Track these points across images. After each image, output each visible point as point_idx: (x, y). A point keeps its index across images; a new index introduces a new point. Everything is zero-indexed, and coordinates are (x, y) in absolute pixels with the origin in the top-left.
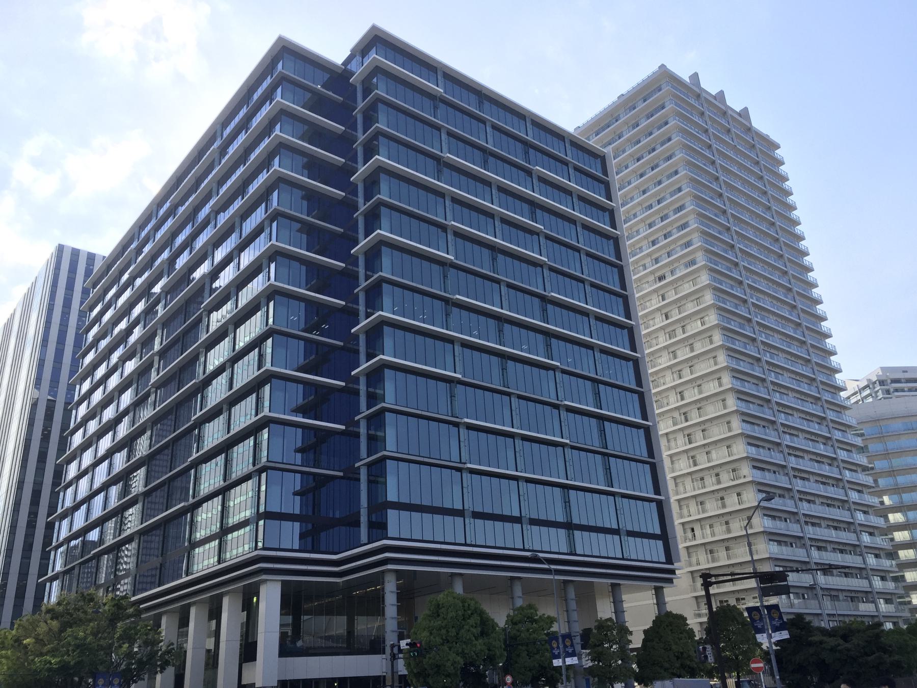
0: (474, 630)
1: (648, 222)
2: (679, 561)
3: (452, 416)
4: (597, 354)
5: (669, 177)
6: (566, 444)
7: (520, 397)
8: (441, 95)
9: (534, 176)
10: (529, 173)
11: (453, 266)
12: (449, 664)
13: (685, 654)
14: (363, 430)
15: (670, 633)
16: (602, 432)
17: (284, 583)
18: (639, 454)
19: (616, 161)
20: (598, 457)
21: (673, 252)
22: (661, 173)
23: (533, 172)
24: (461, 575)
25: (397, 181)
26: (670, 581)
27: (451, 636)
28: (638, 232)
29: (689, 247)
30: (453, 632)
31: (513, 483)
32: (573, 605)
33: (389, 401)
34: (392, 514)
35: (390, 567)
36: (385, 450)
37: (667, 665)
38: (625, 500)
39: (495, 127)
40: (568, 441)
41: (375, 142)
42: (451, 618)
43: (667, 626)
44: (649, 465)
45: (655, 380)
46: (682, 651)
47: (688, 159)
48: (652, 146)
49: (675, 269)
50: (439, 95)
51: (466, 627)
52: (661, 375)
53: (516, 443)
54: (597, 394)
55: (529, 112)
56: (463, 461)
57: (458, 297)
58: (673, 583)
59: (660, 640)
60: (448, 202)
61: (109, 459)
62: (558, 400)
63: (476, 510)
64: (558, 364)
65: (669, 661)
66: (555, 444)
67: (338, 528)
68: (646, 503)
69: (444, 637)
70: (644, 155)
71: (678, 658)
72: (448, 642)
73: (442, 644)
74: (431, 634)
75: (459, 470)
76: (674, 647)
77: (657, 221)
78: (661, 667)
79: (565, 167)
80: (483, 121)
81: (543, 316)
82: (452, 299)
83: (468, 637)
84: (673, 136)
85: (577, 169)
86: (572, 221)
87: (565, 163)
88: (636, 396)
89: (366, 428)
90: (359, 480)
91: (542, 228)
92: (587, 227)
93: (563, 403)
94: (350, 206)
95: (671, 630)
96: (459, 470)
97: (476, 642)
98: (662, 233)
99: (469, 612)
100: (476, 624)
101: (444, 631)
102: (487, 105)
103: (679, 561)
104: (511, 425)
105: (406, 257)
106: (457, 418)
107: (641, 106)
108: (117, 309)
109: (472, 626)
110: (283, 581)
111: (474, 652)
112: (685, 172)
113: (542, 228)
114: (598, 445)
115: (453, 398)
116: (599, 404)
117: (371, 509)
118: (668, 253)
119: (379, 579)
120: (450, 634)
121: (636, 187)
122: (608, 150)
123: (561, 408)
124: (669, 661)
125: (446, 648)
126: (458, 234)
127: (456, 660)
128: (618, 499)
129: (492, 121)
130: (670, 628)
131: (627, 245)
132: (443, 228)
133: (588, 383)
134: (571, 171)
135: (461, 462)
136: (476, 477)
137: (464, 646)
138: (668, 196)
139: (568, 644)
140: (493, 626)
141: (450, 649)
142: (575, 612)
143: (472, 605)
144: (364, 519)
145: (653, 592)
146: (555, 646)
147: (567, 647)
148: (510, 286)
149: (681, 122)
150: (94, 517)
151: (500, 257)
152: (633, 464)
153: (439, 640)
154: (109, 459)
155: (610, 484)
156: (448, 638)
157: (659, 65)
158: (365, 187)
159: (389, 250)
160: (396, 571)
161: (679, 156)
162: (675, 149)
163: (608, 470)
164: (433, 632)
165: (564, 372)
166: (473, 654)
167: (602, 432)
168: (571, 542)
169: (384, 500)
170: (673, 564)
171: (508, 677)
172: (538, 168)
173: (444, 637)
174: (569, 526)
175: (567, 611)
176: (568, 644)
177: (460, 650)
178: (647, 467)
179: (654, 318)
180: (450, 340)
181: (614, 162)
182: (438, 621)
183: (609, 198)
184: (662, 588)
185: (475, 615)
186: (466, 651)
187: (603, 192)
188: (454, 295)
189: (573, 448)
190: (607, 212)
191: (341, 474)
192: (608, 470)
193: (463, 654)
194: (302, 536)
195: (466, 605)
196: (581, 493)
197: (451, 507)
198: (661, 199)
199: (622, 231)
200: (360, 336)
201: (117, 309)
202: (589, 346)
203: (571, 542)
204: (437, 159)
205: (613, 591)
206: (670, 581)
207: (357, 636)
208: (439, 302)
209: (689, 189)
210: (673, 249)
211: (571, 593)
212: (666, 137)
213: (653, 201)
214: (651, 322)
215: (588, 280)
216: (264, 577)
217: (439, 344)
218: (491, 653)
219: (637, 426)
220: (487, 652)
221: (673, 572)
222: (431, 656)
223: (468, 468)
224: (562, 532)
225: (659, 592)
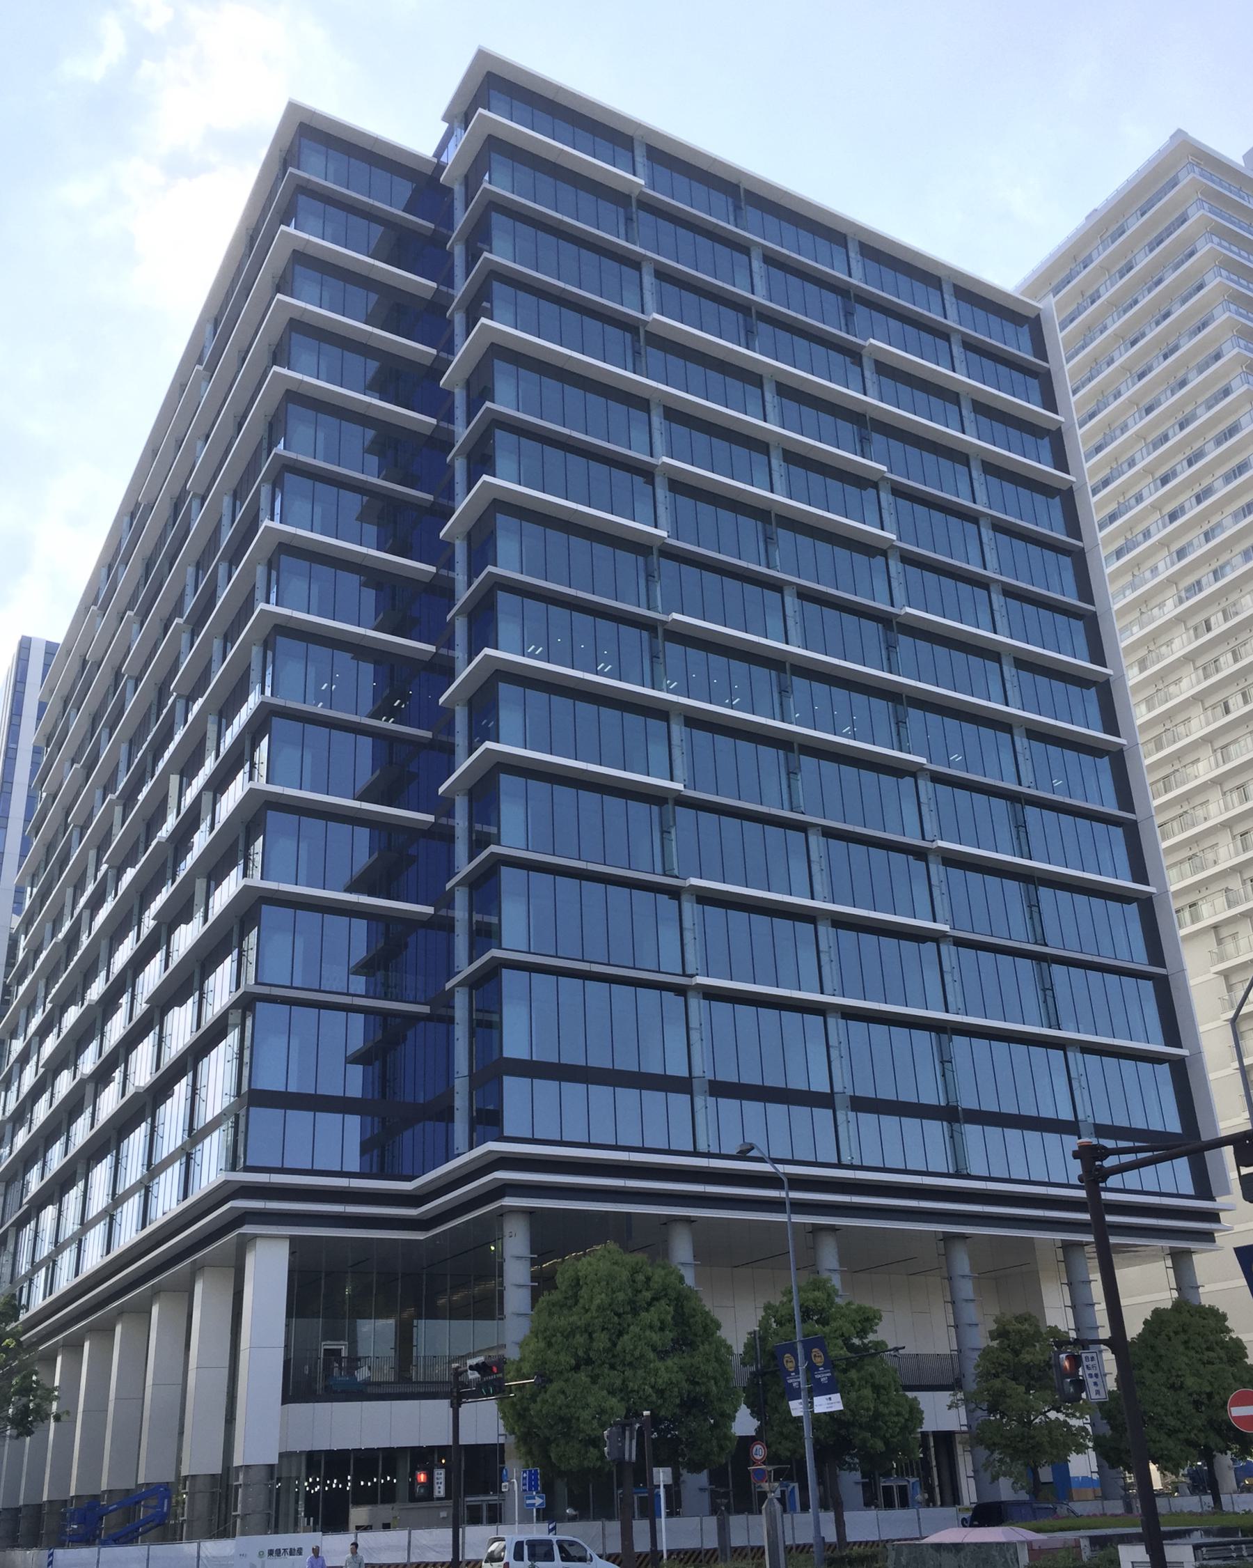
0: (655, 1337)
1: (1176, 546)
2: (1227, 1191)
3: (665, 875)
4: (1021, 742)
5: (1228, 478)
6: (944, 935)
7: (829, 833)
8: (642, 193)
9: (865, 360)
10: (854, 354)
11: (669, 553)
12: (585, 1415)
13: (1217, 1397)
14: (460, 913)
15: (1181, 1349)
16: (1033, 906)
17: (296, 1244)
18: (1127, 957)
19: (1064, 333)
20: (1025, 965)
21: (1228, 569)
22: (1192, 395)
23: (864, 352)
24: (689, 1220)
25: (536, 376)
26: (1208, 1237)
27: (599, 1350)
28: (1154, 570)
29: (1240, 475)
30: (602, 1340)
31: (814, 1021)
32: (966, 1289)
33: (511, 843)
34: (514, 1088)
35: (508, 1201)
36: (500, 947)
37: (1172, 1422)
38: (1092, 1060)
39: (771, 260)
40: (946, 928)
41: (485, 304)
42: (599, 1307)
43: (1176, 1333)
44: (1150, 983)
45: (1195, 855)
46: (1208, 1390)
47: (1243, 324)
48: (1180, 375)
49: (1222, 567)
50: (636, 192)
51: (634, 1329)
52: (1207, 843)
53: (820, 934)
54: (1020, 826)
55: (852, 225)
56: (689, 972)
57: (676, 616)
58: (1213, 1241)
59: (1157, 1364)
60: (657, 420)
61: (190, 1074)
62: (924, 839)
63: (720, 1078)
64: (923, 760)
65: (1179, 1412)
66: (919, 936)
67: (421, 1124)
68: (1145, 1067)
69: (580, 1353)
70: (1171, 433)
71: (1197, 1404)
72: (589, 1361)
73: (576, 1368)
74: (550, 1345)
75: (681, 991)
76: (1190, 1382)
77: (1196, 542)
78: (1160, 1427)
79: (942, 344)
80: (743, 248)
81: (1018, 838)
82: (666, 623)
83: (637, 1353)
84: (1225, 347)
85: (970, 346)
86: (958, 456)
87: (943, 334)
88: (1117, 833)
89: (467, 908)
90: (451, 1020)
91: (884, 468)
92: (993, 469)
93: (934, 845)
94: (440, 442)
95: (1186, 1342)
96: (681, 991)
97: (659, 1364)
98: (1190, 493)
99: (648, 1295)
100: (662, 1322)
101: (580, 1339)
102: (752, 214)
103: (1227, 1191)
104: (313, 454)
105: (555, 536)
106: (677, 877)
107: (1135, 225)
108: (217, 827)
109: (651, 1327)
110: (293, 1240)
111: (653, 1387)
112: (1236, 350)
113: (884, 468)
114: (1024, 938)
115: (665, 835)
116: (1025, 849)
117: (475, 1080)
118: (1215, 572)
119: (492, 1228)
120: (595, 1346)
121: (1148, 471)
122: (1048, 305)
123: (931, 858)
124: (1179, 1412)
125: (583, 1377)
126: (679, 486)
127: (607, 1405)
128: (1075, 1057)
129: (762, 245)
130: (1183, 1337)
131: (1094, 506)
132: (646, 473)
133: (999, 805)
134: (957, 350)
135: (684, 975)
136: (722, 1009)
137: (629, 1373)
138: (1220, 482)
139: (819, 1360)
140: (705, 1328)
141: (594, 1379)
142: (971, 1305)
143: (656, 1278)
144: (461, 1102)
145: (1169, 1263)
146: (790, 1366)
147: (817, 1368)
148: (805, 595)
149: (1241, 315)
150: (204, 1184)
151: (914, 715)
152: (1111, 979)
153: (567, 1359)
154: (190, 1074)
155: (1053, 1022)
156: (592, 1354)
157: (1172, 132)
158: (468, 396)
159: (514, 522)
160: (530, 1212)
161: (1222, 317)
162: (1232, 376)
163: (1047, 989)
164: (553, 1340)
165: (937, 778)
166: (649, 1390)
167: (1033, 906)
168: (956, 1148)
169: (496, 1057)
170: (1212, 1199)
171: (759, 1446)
172: (872, 341)
173: (580, 1353)
174: (950, 1114)
175: (953, 1303)
176: (819, 1360)
177: (618, 1382)
178: (1148, 986)
179: (1189, 719)
180: (659, 712)
181: (1061, 335)
182: (572, 1315)
183: (1050, 404)
184: (1189, 1252)
185: (663, 1302)
186: (631, 1384)
187: (1036, 394)
188: (669, 614)
189: (959, 943)
190: (1047, 440)
191: (426, 1009)
192: (1047, 989)
193: (623, 1391)
194: (365, 1148)
195: (640, 1277)
196: (980, 1044)
197: (660, 1071)
198: (1213, 529)
199: (1081, 475)
200: (457, 708)
201: (217, 827)
202: (1002, 724)
203: (956, 1148)
204: (629, 326)
205: (1067, 1261)
206: (1208, 1237)
207: (425, 1357)
208: (635, 632)
209: (1236, 350)
210: (1228, 563)
211: (962, 1262)
212: (1211, 351)
213: (1187, 497)
214: (1181, 729)
215: (997, 581)
216: (247, 1229)
217: (632, 720)
218: (698, 1389)
219: (1121, 896)
220: (685, 1385)
221: (1213, 1216)
222: (547, 1396)
223: (700, 987)
224: (935, 1129)
225: (1180, 1261)
